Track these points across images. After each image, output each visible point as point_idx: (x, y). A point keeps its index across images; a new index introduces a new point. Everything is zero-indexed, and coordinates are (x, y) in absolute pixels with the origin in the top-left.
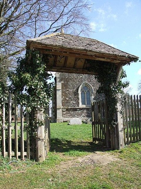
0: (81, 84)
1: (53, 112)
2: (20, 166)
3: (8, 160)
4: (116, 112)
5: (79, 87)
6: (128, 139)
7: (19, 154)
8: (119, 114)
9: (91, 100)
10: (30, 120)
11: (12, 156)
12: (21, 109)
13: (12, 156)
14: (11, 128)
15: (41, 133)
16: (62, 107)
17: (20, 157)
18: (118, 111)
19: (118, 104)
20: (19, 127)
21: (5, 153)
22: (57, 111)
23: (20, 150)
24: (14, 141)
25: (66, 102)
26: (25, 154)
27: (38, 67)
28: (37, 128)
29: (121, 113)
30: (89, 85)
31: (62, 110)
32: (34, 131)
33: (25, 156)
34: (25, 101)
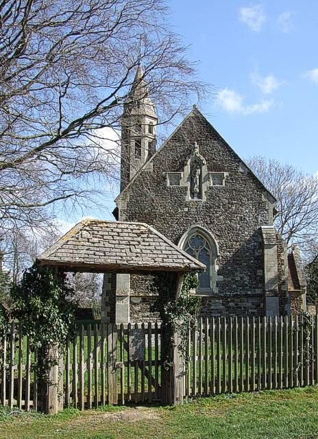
0: (185, 230)
1: (106, 305)
2: (19, 417)
3: (9, 411)
4: (172, 347)
5: (180, 237)
6: (193, 390)
7: (22, 402)
8: (176, 350)
9: (211, 275)
10: (39, 357)
11: (14, 406)
12: (28, 342)
13: (14, 406)
14: (13, 368)
15: (54, 375)
16: (130, 292)
17: (24, 407)
18: (175, 346)
19: (176, 335)
20: (24, 366)
21: (5, 401)
22: (117, 303)
23: (24, 398)
24: (17, 381)
25: (143, 280)
26: (30, 403)
27: (52, 289)
28: (49, 369)
29: (180, 348)
30: (206, 232)
31: (131, 302)
32: (44, 373)
33: (31, 406)
34: (33, 331)
